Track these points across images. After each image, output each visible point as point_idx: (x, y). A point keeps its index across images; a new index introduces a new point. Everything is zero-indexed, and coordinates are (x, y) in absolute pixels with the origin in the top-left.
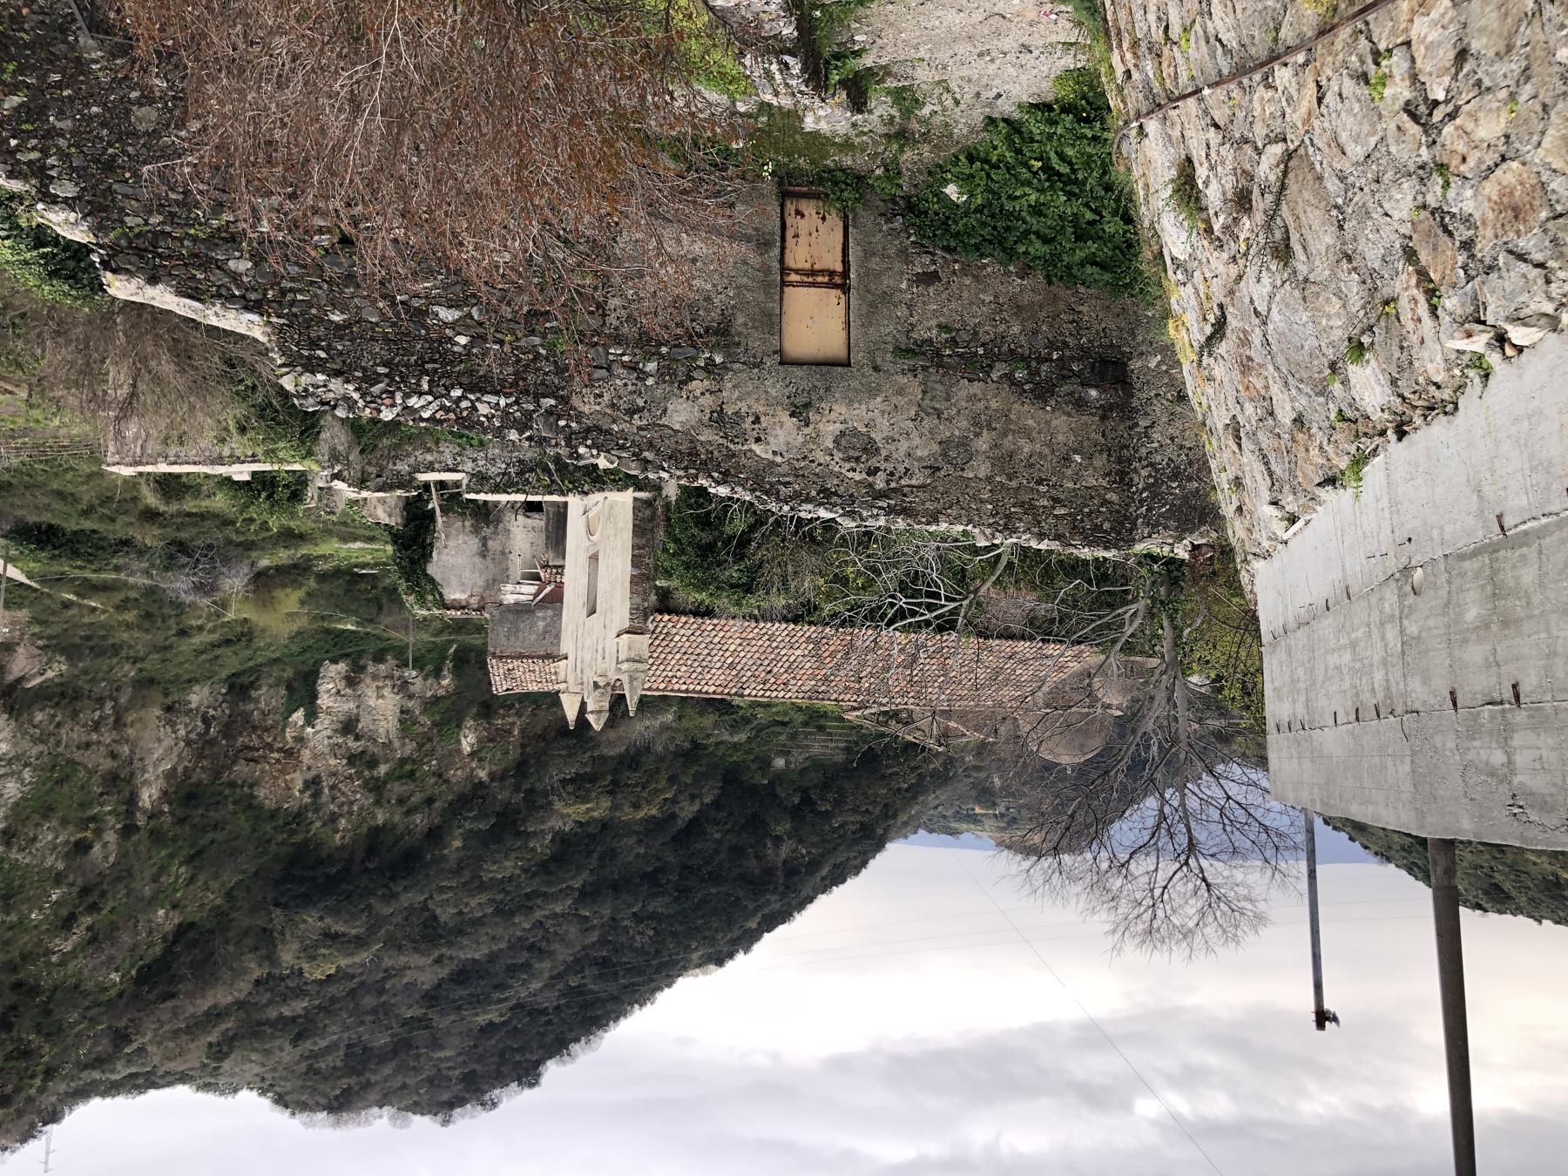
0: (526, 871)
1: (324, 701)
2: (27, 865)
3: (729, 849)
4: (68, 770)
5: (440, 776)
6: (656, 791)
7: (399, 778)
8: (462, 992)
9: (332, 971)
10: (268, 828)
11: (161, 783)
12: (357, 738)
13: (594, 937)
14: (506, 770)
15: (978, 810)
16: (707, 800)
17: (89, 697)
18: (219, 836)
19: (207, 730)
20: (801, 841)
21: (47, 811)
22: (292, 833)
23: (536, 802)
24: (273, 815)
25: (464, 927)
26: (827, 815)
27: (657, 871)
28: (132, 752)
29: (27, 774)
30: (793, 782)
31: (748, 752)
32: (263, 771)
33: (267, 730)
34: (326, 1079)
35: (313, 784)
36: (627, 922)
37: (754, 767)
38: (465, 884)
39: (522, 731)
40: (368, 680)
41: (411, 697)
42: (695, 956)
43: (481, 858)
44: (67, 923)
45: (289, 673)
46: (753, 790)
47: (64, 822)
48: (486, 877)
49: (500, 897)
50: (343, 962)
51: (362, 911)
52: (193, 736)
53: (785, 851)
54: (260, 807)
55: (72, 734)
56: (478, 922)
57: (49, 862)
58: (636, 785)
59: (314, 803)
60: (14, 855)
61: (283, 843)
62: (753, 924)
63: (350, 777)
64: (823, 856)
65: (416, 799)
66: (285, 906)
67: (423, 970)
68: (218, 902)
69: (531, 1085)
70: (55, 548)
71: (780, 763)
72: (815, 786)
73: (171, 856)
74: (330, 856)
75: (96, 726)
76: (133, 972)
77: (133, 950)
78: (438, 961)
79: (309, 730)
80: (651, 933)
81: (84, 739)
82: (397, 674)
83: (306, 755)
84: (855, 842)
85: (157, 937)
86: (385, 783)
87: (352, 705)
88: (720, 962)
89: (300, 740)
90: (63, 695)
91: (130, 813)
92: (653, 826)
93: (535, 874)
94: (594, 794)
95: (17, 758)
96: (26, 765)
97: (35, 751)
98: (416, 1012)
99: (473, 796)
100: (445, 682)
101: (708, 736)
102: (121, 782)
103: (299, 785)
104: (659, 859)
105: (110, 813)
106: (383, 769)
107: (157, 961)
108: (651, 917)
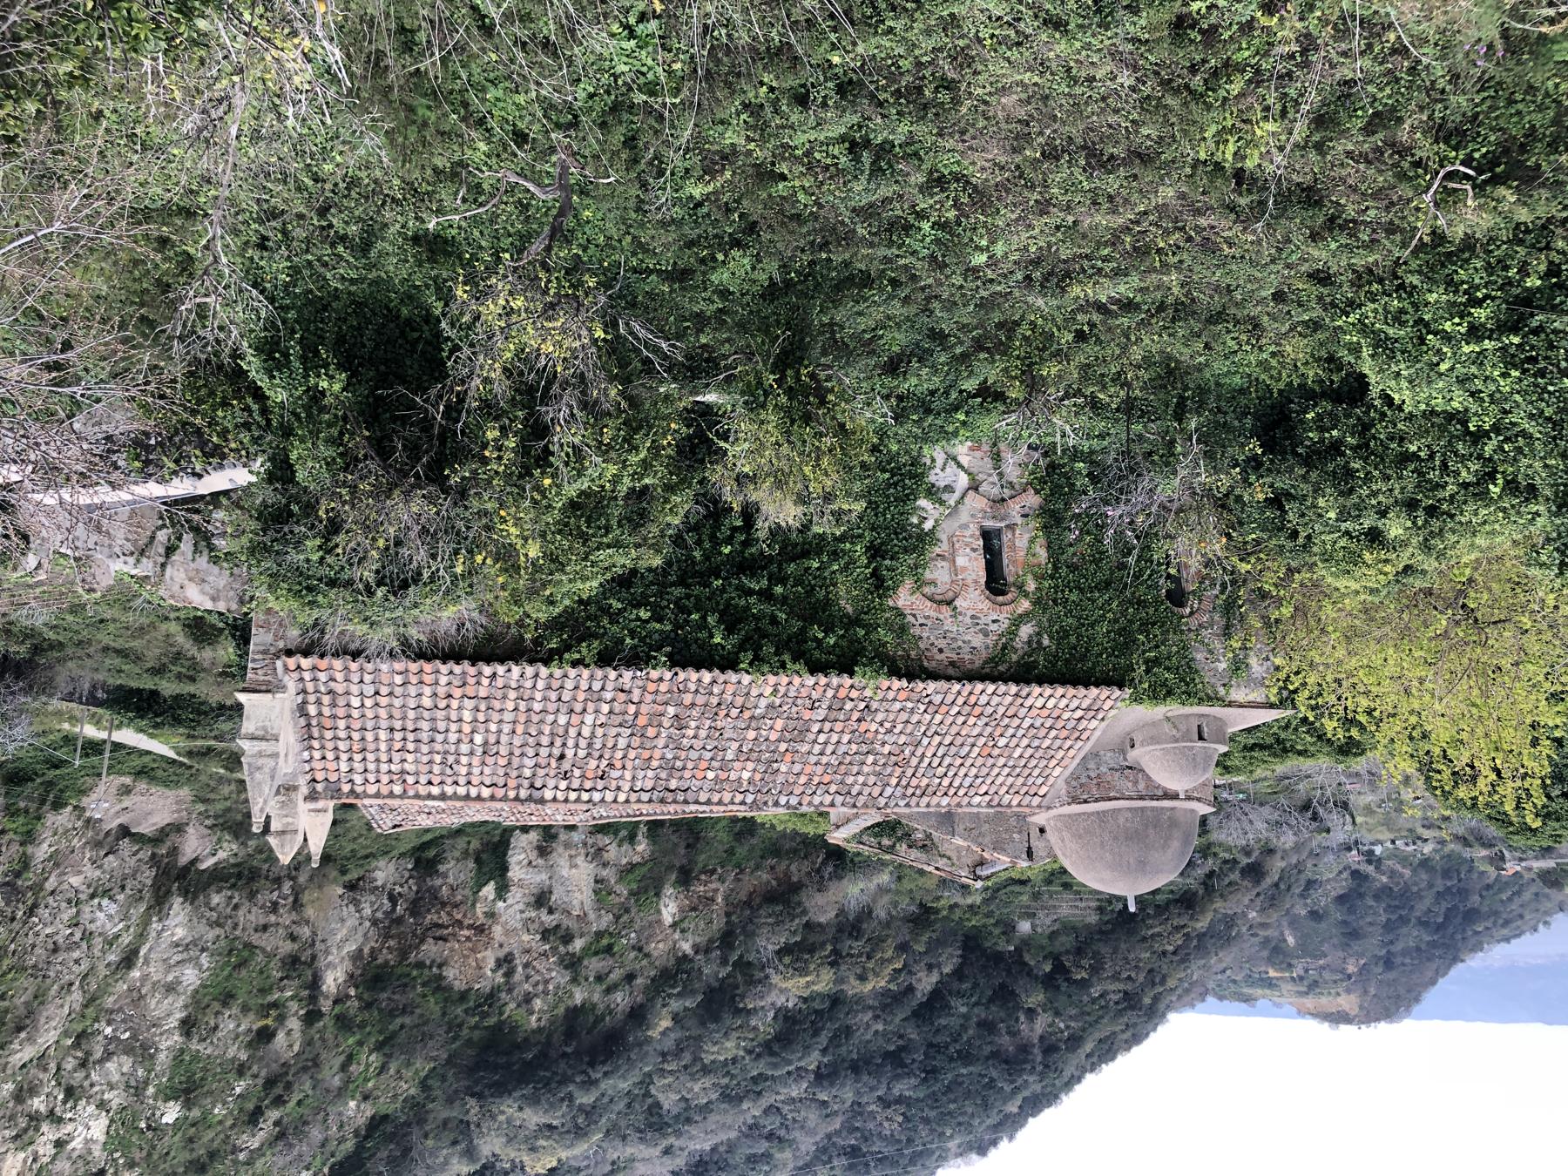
0: (750, 1052)
1: (515, 873)
2: (209, 1057)
3: (979, 1024)
4: (246, 954)
5: (640, 949)
6: (883, 961)
7: (596, 953)
9: (554, 1164)
10: (459, 1011)
11: (347, 965)
12: (551, 911)
13: (837, 1124)
14: (711, 941)
15: (1272, 973)
16: (947, 970)
17: (267, 878)
18: (407, 1020)
19: (394, 909)
20: (1057, 1014)
21: (227, 998)
22: (484, 1015)
23: (749, 974)
24: (463, 996)
25: (688, 1115)
26: (1084, 984)
27: (901, 1049)
28: (314, 933)
29: (205, 960)
30: (1043, 948)
31: (989, 915)
32: (452, 950)
33: (456, 906)
35: (506, 962)
36: (873, 1107)
37: (997, 931)
38: (686, 1067)
39: (726, 898)
40: (560, 849)
41: (605, 865)
42: (952, 1145)
43: (699, 1038)
44: (255, 1117)
45: (475, 844)
46: (998, 957)
47: (245, 1009)
48: (707, 1059)
49: (726, 1081)
50: (564, 1155)
51: (563, 1100)
52: (379, 915)
53: (1041, 1024)
54: (450, 988)
55: (250, 916)
56: (706, 1109)
57: (231, 1053)
58: (860, 955)
59: (507, 983)
60: (194, 1045)
61: (476, 1027)
62: (1012, 1108)
63: (544, 954)
64: (1084, 1030)
65: (615, 976)
66: (479, 1096)
68: (412, 1091)
70: (157, 716)
71: (1025, 927)
72: (1068, 952)
73: (360, 1043)
74: (526, 1040)
75: (275, 907)
76: (326, 1170)
77: (323, 1146)
78: (667, 1151)
79: (500, 904)
80: (900, 1119)
81: (262, 921)
82: (590, 841)
83: (497, 931)
84: (1120, 1013)
85: (348, 1129)
86: (580, 959)
87: (544, 876)
88: (982, 1151)
89: (491, 915)
90: (239, 876)
91: (313, 999)
92: (889, 1001)
93: (759, 1056)
94: (812, 967)
95: (194, 943)
96: (203, 950)
97: (211, 935)
99: (675, 973)
100: (640, 848)
101: (938, 898)
102: (302, 965)
103: (491, 963)
104: (901, 1037)
105: (292, 998)
106: (578, 945)
107: (348, 1158)
108: (900, 1100)
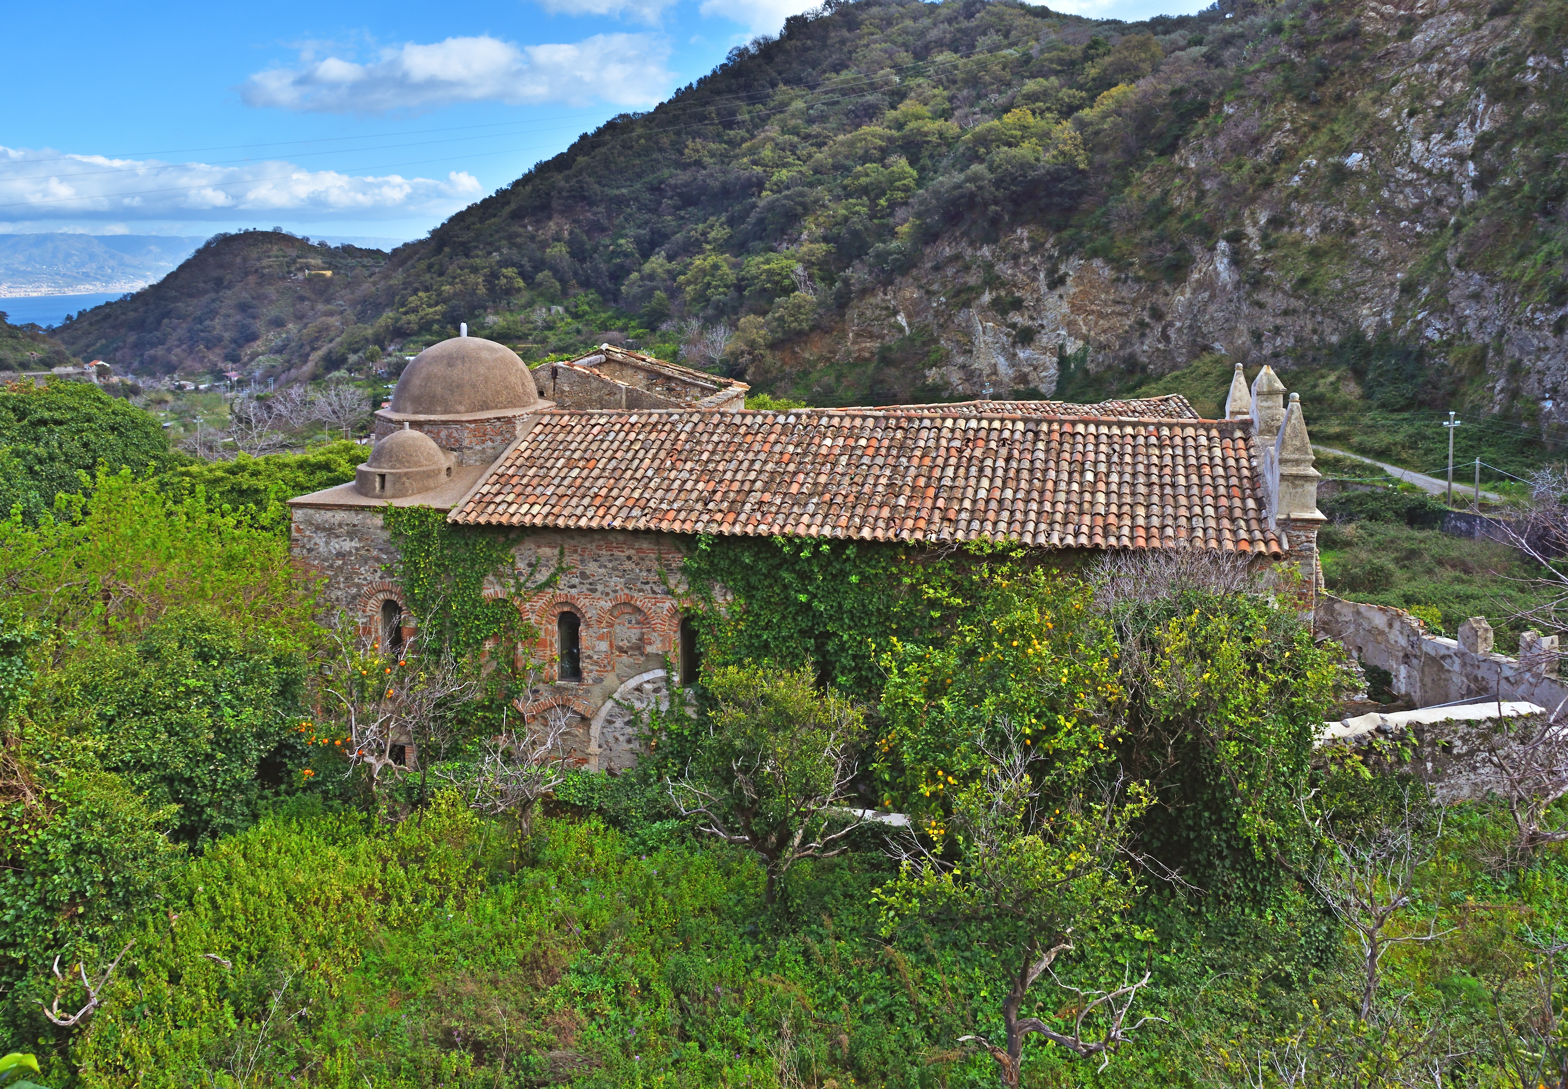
5: (928, 292)
8: (870, 98)
23: (825, 270)
34: (990, 26)
47: (1296, 244)
65: (950, 271)
67: (918, 113)
69: (795, 18)
75: (1277, 330)
81: (1289, 320)
85: (1194, 143)
93: (815, 202)
98: (912, 83)
106: (987, 297)
108: (685, 167)
